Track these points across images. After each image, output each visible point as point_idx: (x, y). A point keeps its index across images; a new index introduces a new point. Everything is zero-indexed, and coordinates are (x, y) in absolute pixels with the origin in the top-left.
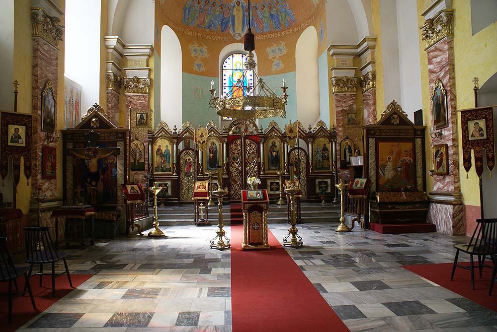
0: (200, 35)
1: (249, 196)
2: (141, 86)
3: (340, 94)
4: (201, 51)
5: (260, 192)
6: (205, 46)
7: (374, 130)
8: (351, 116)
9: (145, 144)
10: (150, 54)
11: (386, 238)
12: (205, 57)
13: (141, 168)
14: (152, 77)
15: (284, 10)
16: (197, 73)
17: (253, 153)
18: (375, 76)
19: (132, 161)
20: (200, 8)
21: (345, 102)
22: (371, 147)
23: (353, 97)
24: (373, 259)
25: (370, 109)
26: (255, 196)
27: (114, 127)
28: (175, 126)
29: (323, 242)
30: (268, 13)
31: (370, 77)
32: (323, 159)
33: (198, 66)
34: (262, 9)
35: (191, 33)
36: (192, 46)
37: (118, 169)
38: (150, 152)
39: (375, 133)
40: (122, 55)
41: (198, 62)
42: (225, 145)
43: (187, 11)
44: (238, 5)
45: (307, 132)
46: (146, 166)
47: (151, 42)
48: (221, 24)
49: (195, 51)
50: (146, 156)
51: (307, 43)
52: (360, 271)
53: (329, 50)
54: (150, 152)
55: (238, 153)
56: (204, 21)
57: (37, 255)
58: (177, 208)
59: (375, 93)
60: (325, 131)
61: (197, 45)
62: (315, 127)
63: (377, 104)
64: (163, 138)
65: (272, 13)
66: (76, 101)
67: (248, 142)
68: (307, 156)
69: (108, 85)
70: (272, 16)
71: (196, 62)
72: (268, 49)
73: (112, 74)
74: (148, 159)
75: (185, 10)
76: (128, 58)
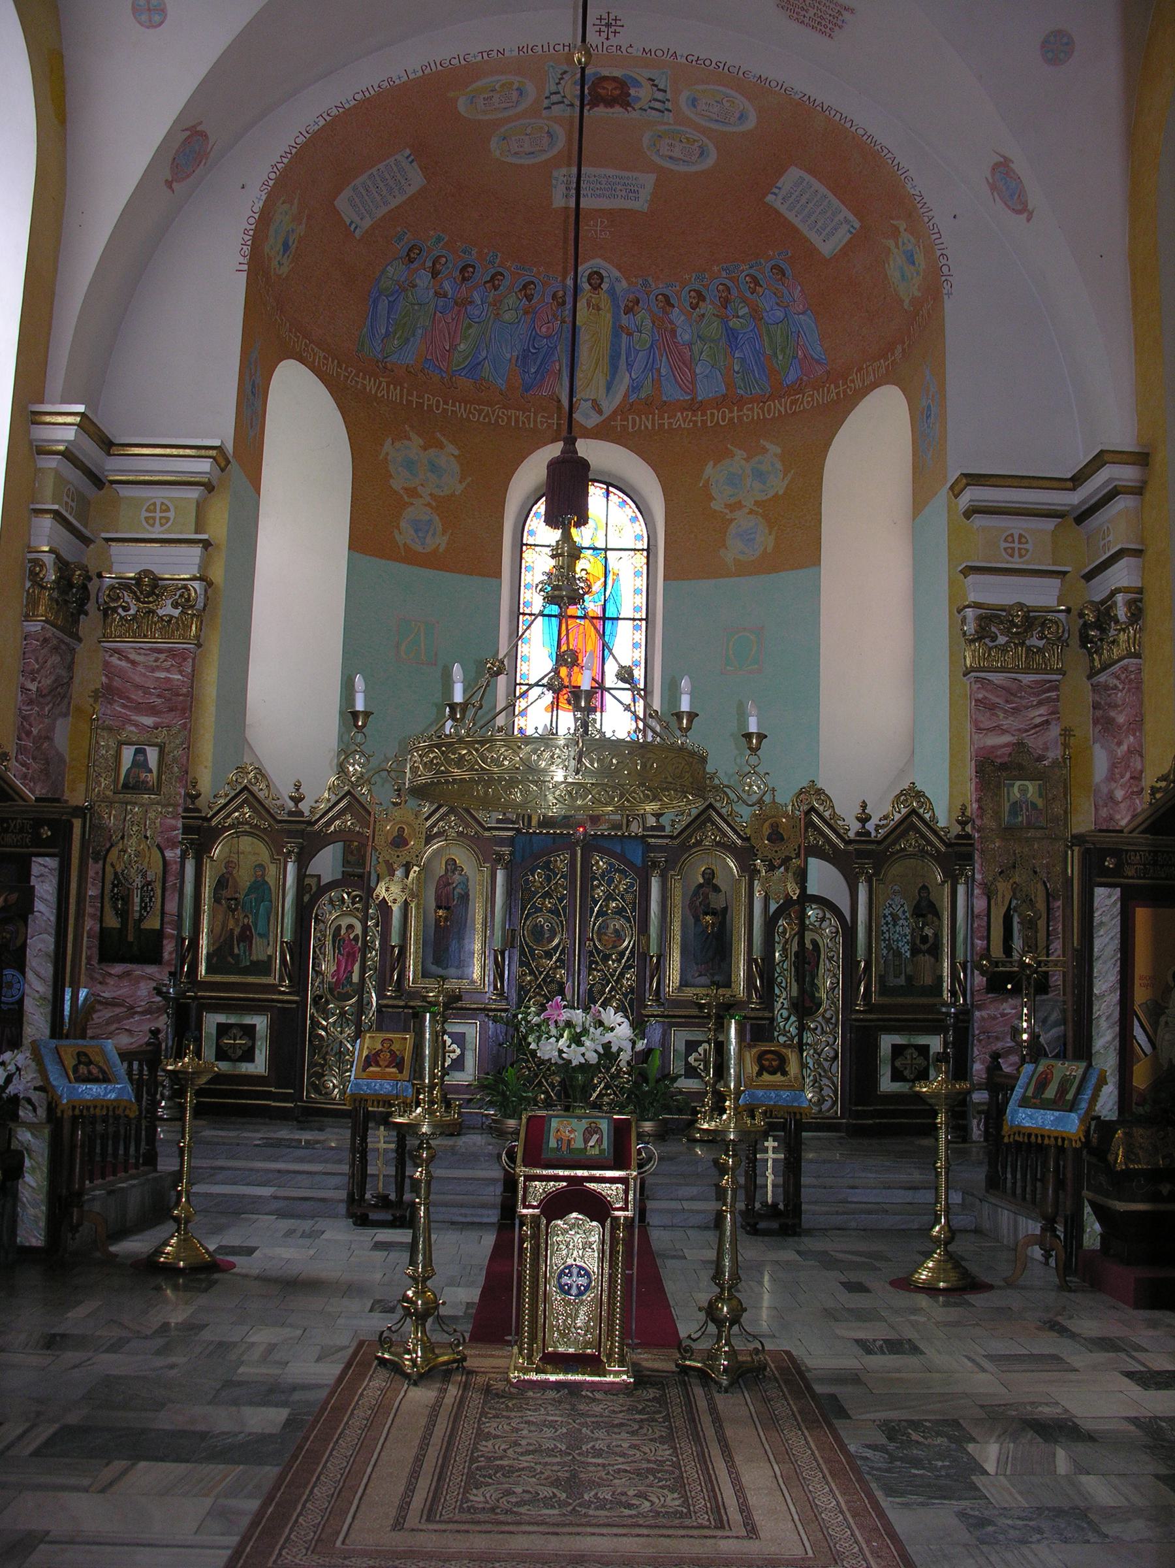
0: (433, 402)
1: (553, 1143)
2: (167, 609)
3: (997, 678)
4: (434, 468)
5: (604, 1125)
6: (451, 448)
7: (1115, 853)
8: (1023, 791)
9: (169, 854)
10: (215, 483)
11: (1143, 1335)
13: (146, 950)
14: (217, 574)
15: (780, 314)
16: (411, 558)
17: (620, 912)
18: (1140, 610)
19: (113, 922)
20: (436, 294)
21: (1016, 711)
22: (1102, 924)
23: (1048, 690)
24: (1061, 1454)
25: (1119, 744)
26: (578, 1144)
27: (24, 798)
28: (298, 787)
29: (866, 1347)
31: (1121, 613)
32: (915, 951)
33: (416, 531)
36: (398, 444)
37: (30, 975)
38: (654, 907)
39: (1119, 868)
40: (98, 481)
42: (500, 876)
43: (383, 304)
44: (596, 288)
45: (851, 834)
46: (169, 948)
47: (220, 429)
48: (525, 357)
50: (172, 907)
51: (870, 457)
52: (990, 1522)
53: (956, 491)
54: (189, 888)
55: (555, 912)
56: (454, 347)
58: (284, 1133)
59: (1140, 682)
60: (924, 829)
61: (417, 441)
62: (882, 810)
63: (1148, 726)
64: (246, 833)
65: (734, 323)
67: (601, 864)
68: (849, 932)
69: (33, 602)
70: (732, 336)
72: (709, 470)
73: (49, 560)
74: (180, 916)
76: (125, 492)
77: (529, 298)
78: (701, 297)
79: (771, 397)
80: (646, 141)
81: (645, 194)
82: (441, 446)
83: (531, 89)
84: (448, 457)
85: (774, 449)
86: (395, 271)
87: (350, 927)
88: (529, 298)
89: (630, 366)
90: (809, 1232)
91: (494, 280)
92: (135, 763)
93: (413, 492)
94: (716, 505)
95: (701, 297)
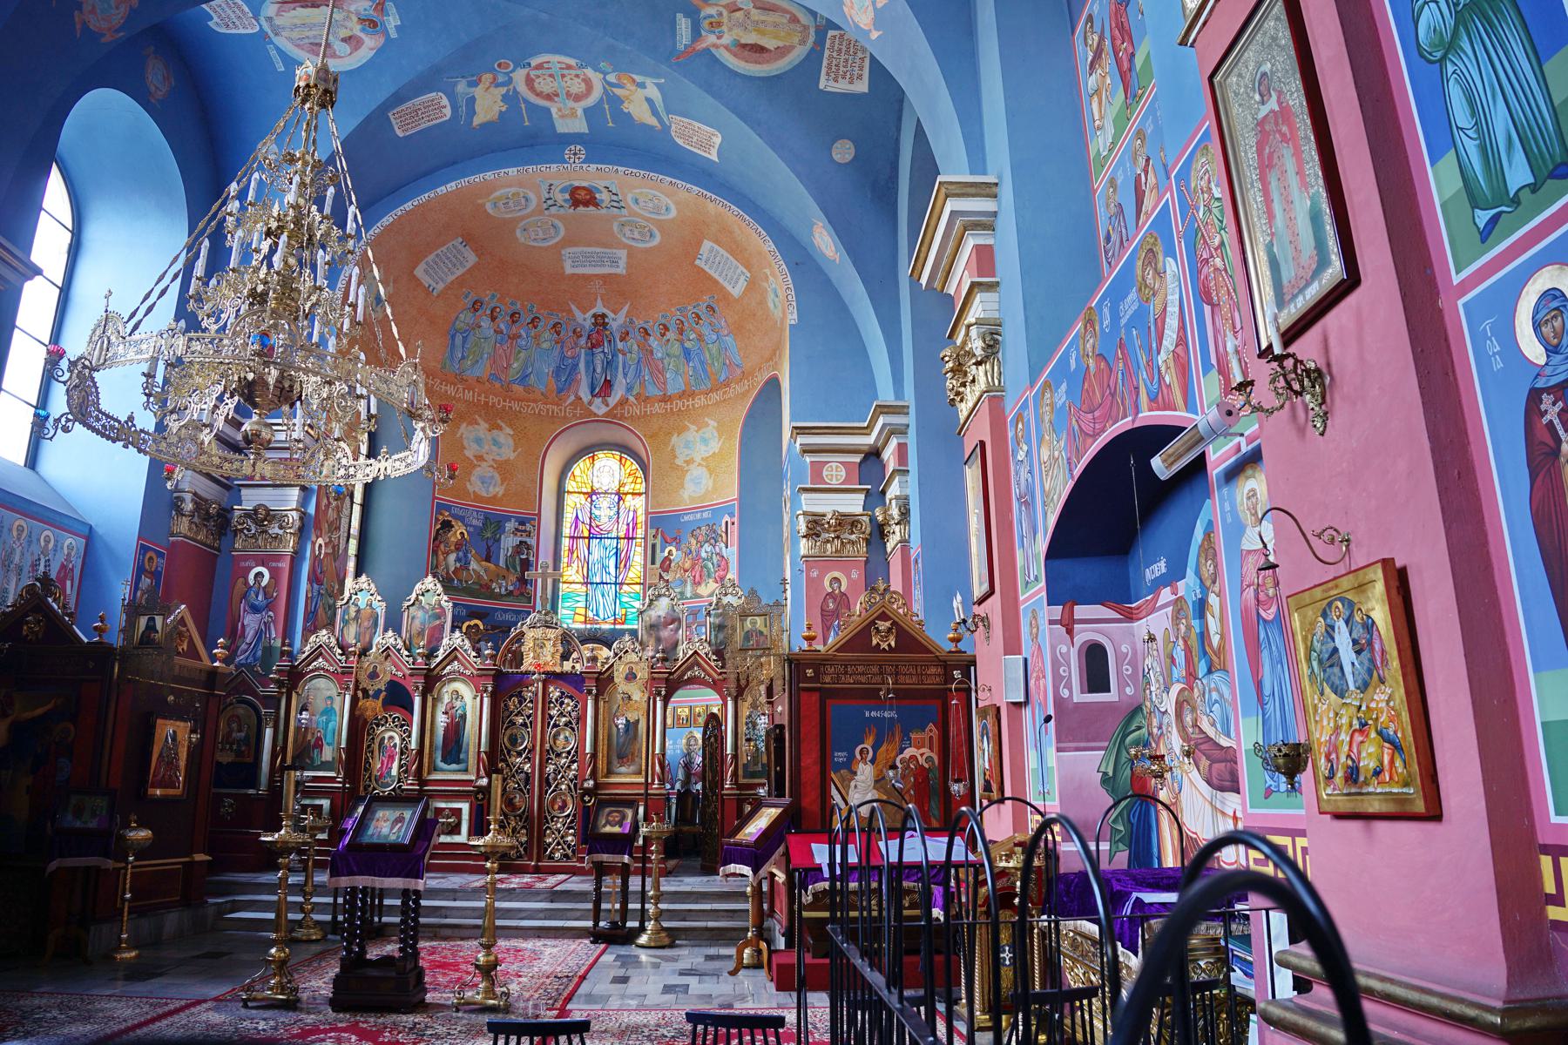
2: (275, 530)
4: (495, 442)
6: (509, 431)
12: (504, 458)
30: (677, 345)
34: (663, 335)
35: (469, 395)
41: (483, 470)
42: (486, 700)
48: (558, 372)
49: (478, 441)
55: (524, 725)
56: (509, 365)
57: (716, 1035)
65: (688, 345)
66: (63, 566)
70: (687, 353)
71: (477, 472)
72: (674, 439)
73: (188, 497)
75: (453, 337)
77: (558, 333)
78: (666, 328)
79: (711, 391)
80: (615, 228)
81: (622, 263)
82: (500, 428)
83: (532, 196)
84: (505, 436)
85: (713, 423)
86: (466, 318)
87: (391, 738)
88: (558, 333)
89: (625, 375)
90: (301, 1010)
91: (534, 322)
92: (148, 627)
93: (480, 458)
94: (679, 462)
95: (666, 328)
